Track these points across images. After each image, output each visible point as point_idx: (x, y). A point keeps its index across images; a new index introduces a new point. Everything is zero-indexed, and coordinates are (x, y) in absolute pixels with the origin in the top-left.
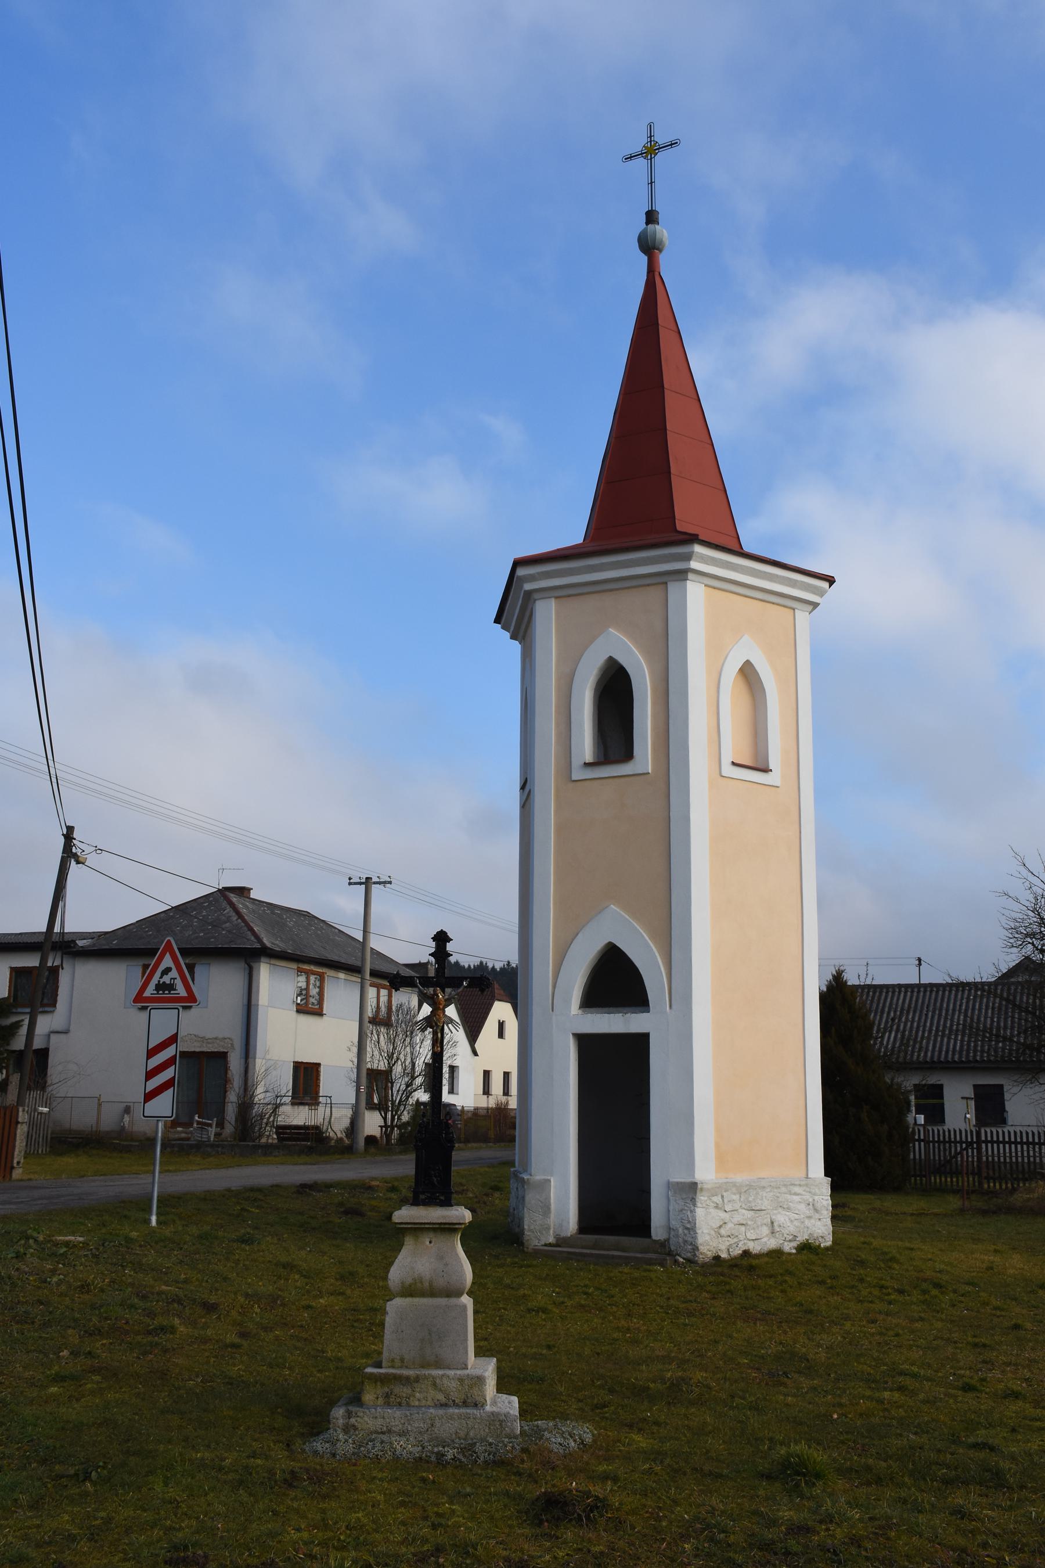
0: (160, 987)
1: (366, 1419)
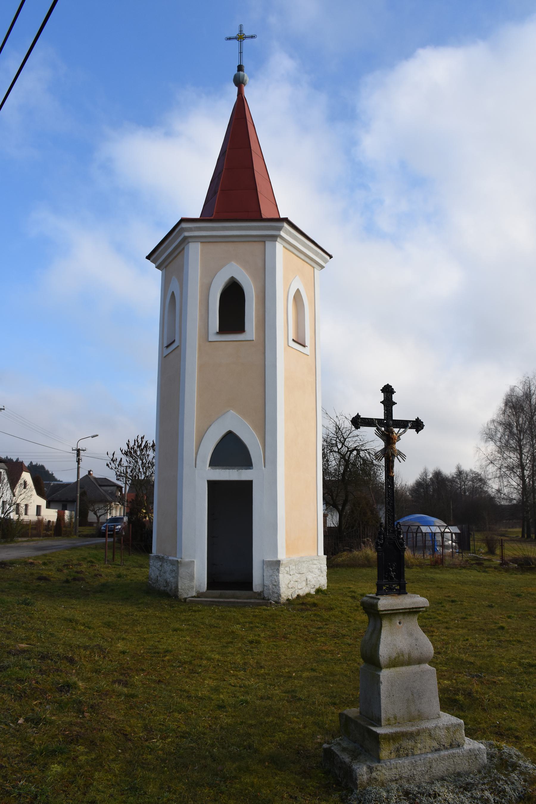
1: (384, 771)
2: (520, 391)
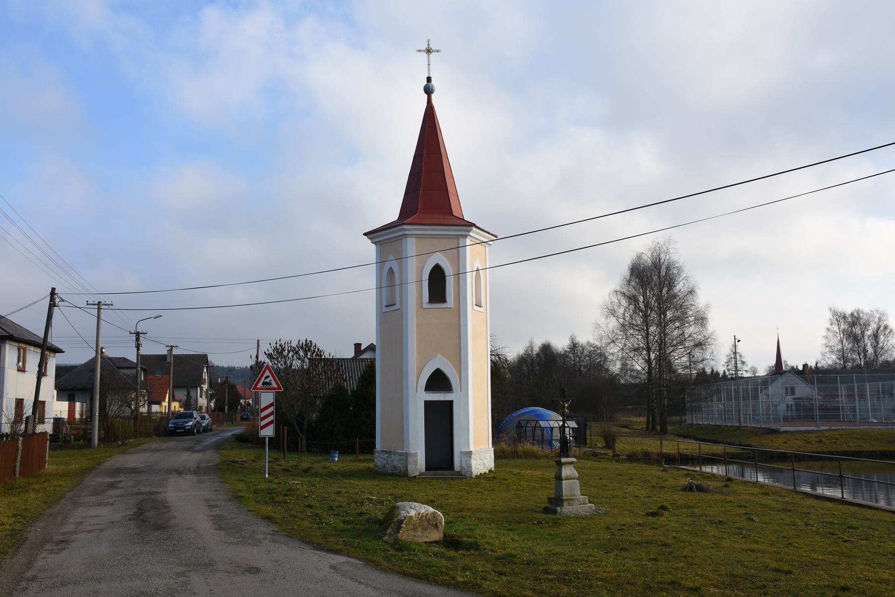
0: (264, 384)
2: (647, 259)
